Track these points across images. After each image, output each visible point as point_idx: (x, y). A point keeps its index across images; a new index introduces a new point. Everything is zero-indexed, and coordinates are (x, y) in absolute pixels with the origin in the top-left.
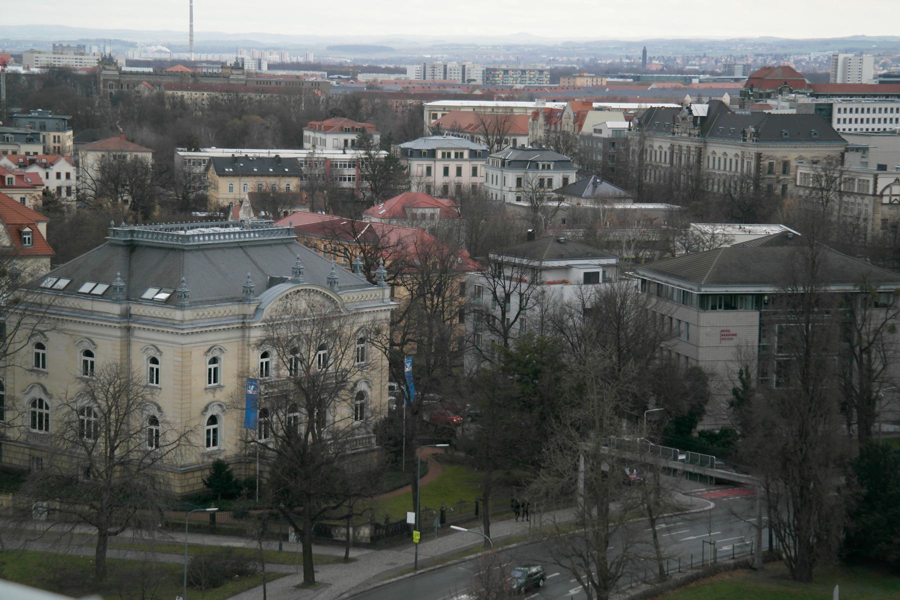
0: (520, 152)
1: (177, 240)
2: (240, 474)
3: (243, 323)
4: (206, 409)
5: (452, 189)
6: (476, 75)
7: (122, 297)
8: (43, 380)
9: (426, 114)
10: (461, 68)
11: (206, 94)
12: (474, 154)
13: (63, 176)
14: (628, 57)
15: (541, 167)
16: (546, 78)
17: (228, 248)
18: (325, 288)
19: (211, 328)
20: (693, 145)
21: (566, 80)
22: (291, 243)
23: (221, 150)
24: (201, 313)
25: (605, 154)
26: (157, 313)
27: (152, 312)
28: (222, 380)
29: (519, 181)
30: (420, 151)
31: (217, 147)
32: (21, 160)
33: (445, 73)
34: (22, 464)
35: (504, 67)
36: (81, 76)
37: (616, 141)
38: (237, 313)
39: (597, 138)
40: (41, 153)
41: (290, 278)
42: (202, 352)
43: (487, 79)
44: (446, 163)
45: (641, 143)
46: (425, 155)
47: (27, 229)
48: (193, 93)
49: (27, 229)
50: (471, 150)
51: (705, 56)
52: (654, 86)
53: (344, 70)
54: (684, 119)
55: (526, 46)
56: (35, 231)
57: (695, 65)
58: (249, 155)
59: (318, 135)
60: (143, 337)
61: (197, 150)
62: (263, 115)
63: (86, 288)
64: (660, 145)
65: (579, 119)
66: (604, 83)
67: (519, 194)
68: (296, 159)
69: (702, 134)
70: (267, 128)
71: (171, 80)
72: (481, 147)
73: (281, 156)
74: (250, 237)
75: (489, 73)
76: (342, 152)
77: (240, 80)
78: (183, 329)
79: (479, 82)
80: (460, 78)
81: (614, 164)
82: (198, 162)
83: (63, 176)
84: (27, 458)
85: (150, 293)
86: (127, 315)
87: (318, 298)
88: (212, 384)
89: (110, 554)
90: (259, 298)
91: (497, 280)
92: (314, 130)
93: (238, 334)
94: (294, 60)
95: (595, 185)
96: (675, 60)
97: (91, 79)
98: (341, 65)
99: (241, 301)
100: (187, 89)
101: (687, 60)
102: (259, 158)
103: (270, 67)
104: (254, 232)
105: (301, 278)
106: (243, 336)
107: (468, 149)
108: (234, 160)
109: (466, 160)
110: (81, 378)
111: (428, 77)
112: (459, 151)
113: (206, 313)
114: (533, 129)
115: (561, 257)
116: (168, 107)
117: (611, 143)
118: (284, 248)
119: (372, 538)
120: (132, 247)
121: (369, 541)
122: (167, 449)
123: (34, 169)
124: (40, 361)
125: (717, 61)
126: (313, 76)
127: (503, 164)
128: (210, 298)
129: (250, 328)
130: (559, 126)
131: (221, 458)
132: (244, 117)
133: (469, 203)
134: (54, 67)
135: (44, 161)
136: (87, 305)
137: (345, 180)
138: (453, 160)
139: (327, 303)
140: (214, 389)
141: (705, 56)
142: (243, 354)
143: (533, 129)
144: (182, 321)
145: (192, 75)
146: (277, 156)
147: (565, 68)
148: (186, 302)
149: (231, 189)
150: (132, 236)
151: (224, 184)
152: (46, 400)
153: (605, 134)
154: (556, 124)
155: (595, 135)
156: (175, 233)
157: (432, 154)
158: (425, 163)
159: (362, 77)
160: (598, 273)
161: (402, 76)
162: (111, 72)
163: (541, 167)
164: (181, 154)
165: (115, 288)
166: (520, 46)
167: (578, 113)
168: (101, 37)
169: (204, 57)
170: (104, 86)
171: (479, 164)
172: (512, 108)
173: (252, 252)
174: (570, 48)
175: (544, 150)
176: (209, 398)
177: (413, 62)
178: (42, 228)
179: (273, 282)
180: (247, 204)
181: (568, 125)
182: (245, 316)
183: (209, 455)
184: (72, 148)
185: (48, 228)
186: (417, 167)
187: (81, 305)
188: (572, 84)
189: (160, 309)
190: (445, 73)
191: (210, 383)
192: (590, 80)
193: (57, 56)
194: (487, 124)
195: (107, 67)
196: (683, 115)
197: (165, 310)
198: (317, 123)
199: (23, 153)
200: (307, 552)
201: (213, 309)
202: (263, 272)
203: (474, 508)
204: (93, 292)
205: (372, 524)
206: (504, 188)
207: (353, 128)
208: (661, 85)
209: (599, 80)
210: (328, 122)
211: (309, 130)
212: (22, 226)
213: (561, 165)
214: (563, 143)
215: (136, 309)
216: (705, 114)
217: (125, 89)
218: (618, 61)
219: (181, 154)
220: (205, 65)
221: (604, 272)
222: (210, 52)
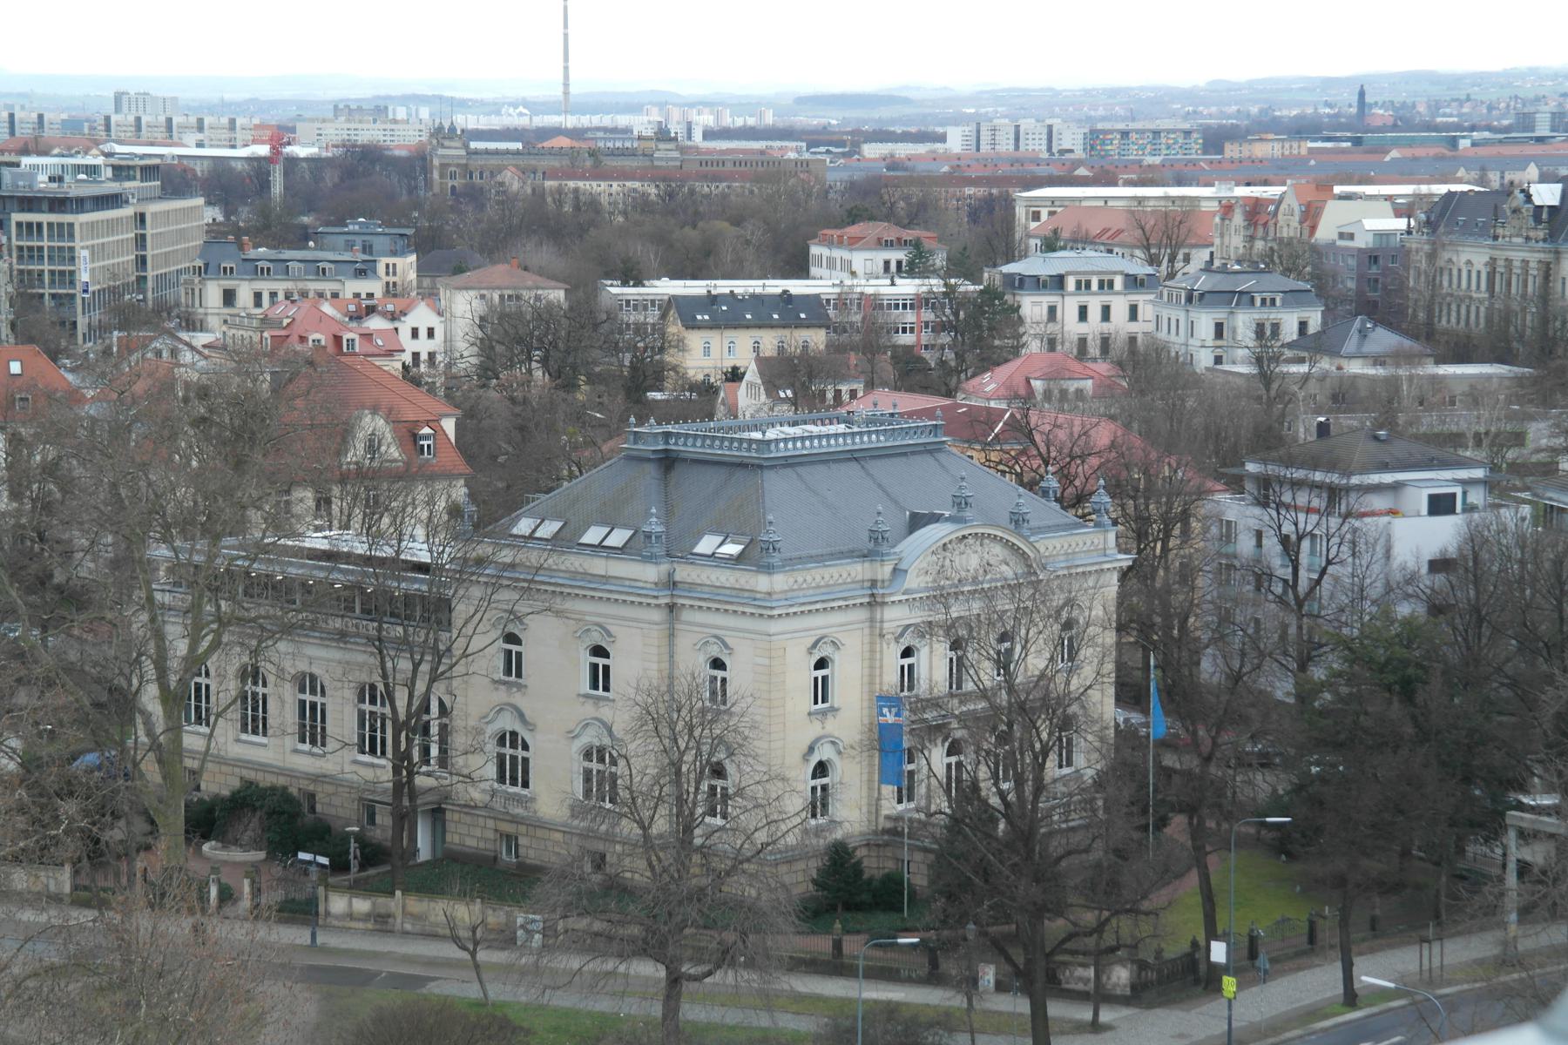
0: (1219, 277)
1: (749, 450)
2: (874, 866)
3: (873, 595)
4: (811, 749)
5: (1118, 346)
6: (1072, 139)
7: (659, 550)
8: (518, 699)
9: (1020, 212)
10: (1045, 131)
11: (615, 184)
12: (1134, 283)
13: (423, 333)
14: (1327, 104)
15: (1258, 302)
16: (1196, 142)
17: (834, 461)
18: (1005, 529)
19: (818, 606)
20: (1534, 258)
21: (1236, 147)
22: (939, 450)
23: (681, 283)
24: (800, 579)
25: (1361, 277)
26: (723, 579)
27: (713, 577)
28: (836, 697)
29: (1219, 330)
30: (1037, 278)
31: (671, 278)
32: (352, 308)
33: (1017, 139)
34: (482, 845)
35: (1121, 126)
36: (395, 161)
37: (1380, 258)
38: (859, 577)
39: (1347, 249)
40: (378, 294)
41: (947, 514)
42: (804, 649)
43: (1092, 148)
44: (1083, 299)
45: (1432, 256)
46: (1045, 286)
47: (426, 430)
48: (594, 184)
49: (426, 430)
50: (1127, 275)
51: (1468, 99)
52: (1394, 154)
53: (836, 137)
54: (1516, 211)
55: (1142, 89)
56: (439, 432)
57: (1451, 115)
58: (737, 291)
59: (837, 253)
60: (698, 623)
61: (639, 283)
62: (737, 221)
63: (593, 536)
64: (1470, 259)
65: (1311, 215)
66: (1304, 152)
67: (1219, 352)
68: (817, 296)
69: (1552, 236)
70: (748, 242)
71: (555, 163)
72: (1141, 269)
73: (793, 291)
74: (862, 442)
75: (1095, 138)
76: (888, 282)
77: (672, 159)
78: (772, 608)
79: (1079, 153)
80: (1044, 147)
81: (1376, 291)
82: (642, 305)
83: (423, 333)
84: (490, 835)
85: (706, 545)
86: (671, 584)
87: (997, 549)
88: (820, 705)
89: (692, 1012)
90: (896, 550)
91: (1283, 512)
92: (830, 243)
93: (862, 614)
94: (739, 122)
95: (1363, 334)
96: (1414, 106)
97: (417, 163)
98: (825, 129)
99: (866, 556)
100: (583, 178)
101: (1435, 106)
102: (754, 296)
103: (708, 134)
104: (869, 433)
105: (968, 514)
106: (872, 620)
107: (1121, 273)
108: (712, 300)
109: (1118, 293)
110: (587, 696)
111: (985, 148)
112: (1106, 278)
113: (809, 579)
114: (1222, 235)
115: (1385, 467)
116: (567, 208)
117: (1372, 257)
118: (928, 459)
119: (1133, 987)
120: (668, 462)
121: (1128, 992)
122: (784, 827)
123: (375, 323)
124: (513, 665)
125: (1490, 108)
126: (792, 151)
127: (1189, 299)
128: (813, 552)
129: (884, 604)
130: (1272, 230)
131: (838, 835)
132: (701, 224)
133: (1144, 368)
134: (354, 146)
135: (390, 307)
136: (598, 566)
137: (904, 330)
138: (1095, 294)
139: (1012, 560)
140: (824, 713)
141: (1468, 99)
142: (872, 651)
143: (1222, 235)
144: (769, 594)
145: (594, 154)
146: (785, 292)
147: (1221, 126)
148: (776, 559)
149: (707, 351)
150: (667, 443)
151: (695, 340)
152: (523, 733)
153: (1362, 242)
154: (1265, 225)
155: (1340, 243)
156: (746, 435)
157: (1058, 282)
158: (1046, 300)
159: (872, 151)
160: (1454, 495)
161: (939, 146)
162: (454, 151)
163: (1258, 302)
164: (614, 290)
165: (648, 536)
166: (1132, 89)
167: (1309, 205)
168: (409, 91)
169: (595, 120)
170: (442, 176)
171: (1141, 299)
172: (1197, 199)
173: (877, 467)
174: (1220, 92)
175: (1262, 271)
176: (815, 729)
177: (957, 120)
178: (449, 426)
179: (917, 522)
180: (752, 375)
181: (1288, 226)
182: (874, 583)
183: (818, 831)
184: (415, 283)
185: (459, 427)
186: (1032, 307)
187: (586, 565)
188: (1246, 154)
189: (728, 572)
190: (1017, 139)
191: (816, 702)
192: (1277, 146)
193: (352, 126)
194: (1147, 228)
195: (447, 143)
196: (1514, 204)
197: (738, 574)
198: (836, 233)
199: (349, 295)
200: (1039, 1014)
201: (821, 571)
202: (896, 502)
203: (1306, 930)
204: (606, 543)
205: (1133, 962)
206: (1191, 341)
207: (899, 239)
208: (1408, 152)
209: (1295, 145)
210: (853, 230)
211: (821, 243)
212: (417, 424)
213: (1294, 298)
214: (1301, 264)
215: (684, 573)
216: (1555, 201)
217: (477, 180)
218: (1310, 111)
219: (614, 290)
220: (600, 134)
221: (1465, 493)
222: (594, 112)
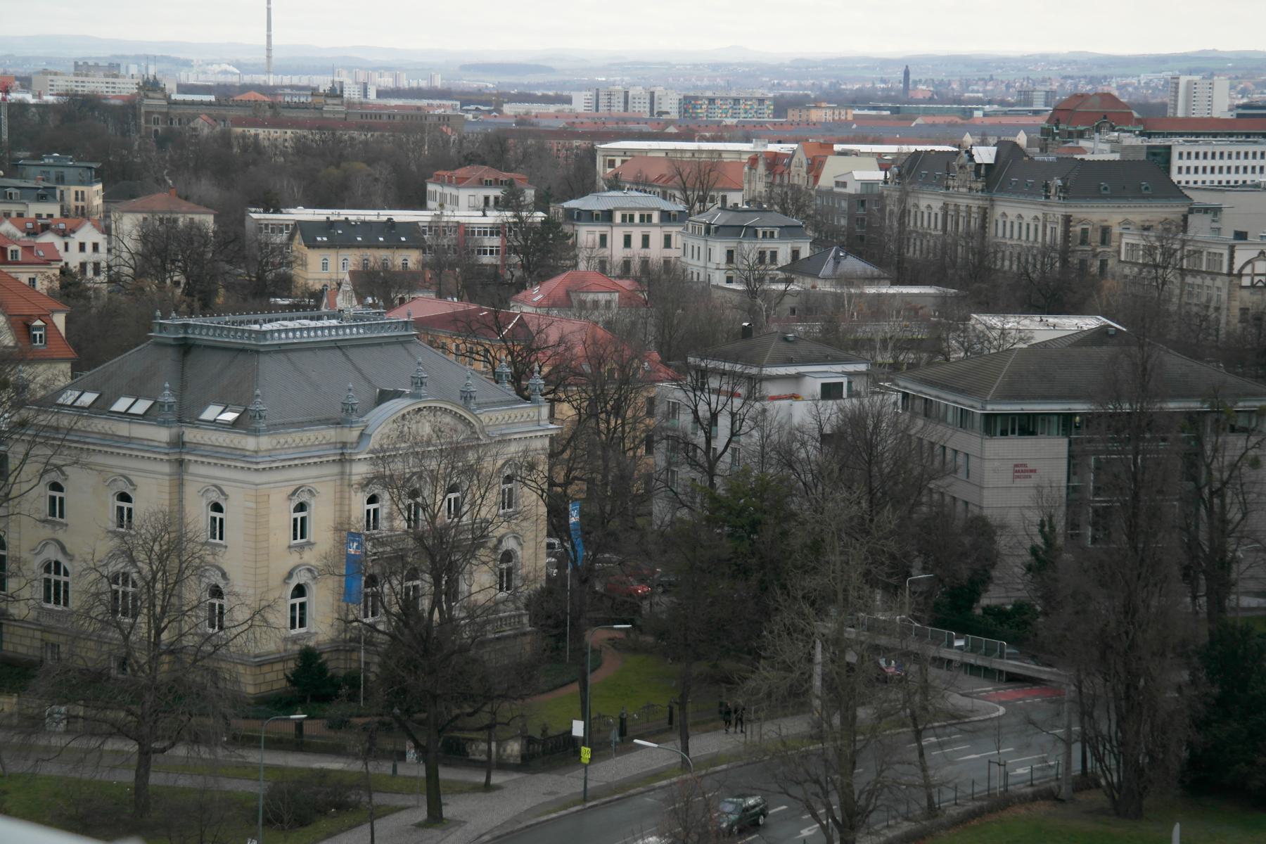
0: (731, 214)
1: (249, 338)
2: (337, 666)
3: (342, 454)
4: (290, 575)
5: (636, 266)
6: (670, 105)
7: (171, 417)
8: (61, 535)
9: (600, 161)
10: (648, 96)
11: (289, 132)
12: (667, 217)
13: (89, 248)
14: (883, 81)
15: (760, 235)
16: (768, 109)
17: (320, 349)
18: (458, 405)
19: (296, 462)
20: (975, 204)
21: (797, 112)
22: (410, 342)
23: (311, 211)
24: (282, 441)
25: (851, 217)
26: (221, 440)
27: (213, 438)
28: (312, 534)
29: (730, 254)
30: (590, 212)
31: (306, 207)
32: (30, 225)
33: (626, 102)
34: (31, 652)
35: (709, 94)
36: (113, 107)
37: (867, 199)
38: (333, 440)
39: (840, 194)
40: (57, 215)
41: (408, 391)
42: (285, 495)
43: (686, 111)
44: (628, 229)
45: (902, 201)
46: (597, 219)
47: (38, 323)
48: (272, 131)
49: (38, 323)
50: (662, 211)
51: (991, 78)
52: (919, 121)
53: (484, 98)
54: (962, 167)
55: (739, 64)
56: (50, 326)
57: (978, 92)
58: (350, 218)
59: (448, 190)
60: (201, 473)
61: (277, 211)
62: (370, 162)
63: (121, 405)
64: (929, 204)
65: (815, 167)
66: (850, 117)
67: (730, 273)
68: (416, 223)
69: (988, 188)
70: (376, 180)
71: (240, 113)
72: (677, 206)
73: (396, 219)
74: (351, 333)
75: (688, 103)
76: (481, 213)
77: (338, 112)
78: (257, 463)
79: (674, 115)
80: (647, 109)
81: (864, 230)
82: (278, 228)
83: (89, 248)
84: (38, 644)
85: (211, 413)
86: (178, 443)
87: (448, 419)
88: (299, 541)
89: (155, 779)
90: (364, 419)
91: (698, 393)
92: (442, 183)
93: (335, 469)
94: (414, 84)
95: (837, 260)
96: (949, 84)
97: (128, 111)
98: (480, 92)
99: (338, 423)
100: (262, 126)
101: (966, 84)
102: (364, 223)
103: (380, 94)
104: (357, 326)
105: (423, 391)
106: (342, 473)
107: (658, 209)
108: (329, 225)
109: (655, 225)
110: (114, 532)
111: (602, 109)
112: (646, 213)
113: (290, 440)
114: (749, 182)
115: (789, 362)
116: (236, 150)
117: (860, 201)
118: (399, 348)
119: (523, 757)
120: (185, 347)
121: (519, 761)
122: (235, 631)
123: (48, 238)
124: (56, 508)
125: (1008, 86)
126: (440, 107)
127: (708, 231)
128: (295, 419)
129: (352, 461)
130: (786, 178)
131: (311, 644)
132: (344, 165)
133: (660, 285)
134: (76, 95)
135: (62, 226)
136: (123, 429)
137: (485, 253)
138: (637, 225)
139: (460, 427)
140: (302, 547)
141: (991, 78)
142: (342, 498)
143: (749, 182)
144: (256, 452)
145: (270, 106)
146: (389, 220)
147: (795, 95)
148: (262, 425)
149: (325, 266)
150: (186, 332)
151: (314, 258)
152: (65, 563)
153: (852, 189)
154: (781, 174)
155: (837, 190)
156: (246, 327)
157: (607, 216)
158: (598, 230)
159: (509, 109)
160: (841, 384)
161: (566, 107)
162: (156, 102)
163: (760, 235)
164: (255, 216)
165: (162, 405)
166: (731, 64)
167: (813, 159)
168: (141, 53)
169: (286, 80)
170: (147, 122)
171: (674, 230)
172: (720, 152)
173: (354, 354)
174: (801, 67)
175: (765, 210)
176: (294, 559)
177: (580, 87)
178: (59, 320)
179: (384, 396)
180: (347, 287)
181: (798, 176)
182: (344, 445)
183: (295, 640)
184: (101, 208)
185: (68, 321)
186: (587, 234)
187: (114, 428)
188: (804, 118)
189: (225, 435)
190: (626, 102)
191: (295, 538)
192: (829, 112)
193: (80, 79)
194: (685, 174)
195: (151, 94)
196: (961, 162)
197: (232, 436)
198: (446, 174)
199: (32, 215)
200: (432, 777)
201: (300, 434)
202: (369, 382)
203: (667, 715)
204: (131, 411)
205: (523, 737)
206: (709, 265)
207: (496, 180)
208: (930, 120)
209: (843, 112)
210: (461, 172)
211: (435, 182)
212: (31, 317)
213: (789, 232)
214: (791, 202)
215: (191, 435)
216: (991, 160)
217: (176, 125)
218: (869, 85)
219: (255, 216)
220: (288, 91)
221: (850, 383)
222: (295, 73)
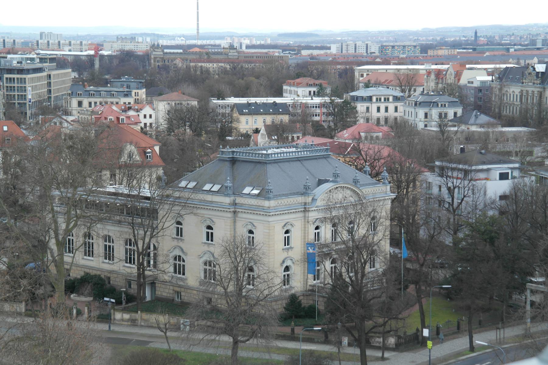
0: (426, 97)
1: (262, 157)
2: (305, 302)
3: (305, 208)
4: (283, 262)
5: (391, 121)
6: (374, 49)
7: (230, 192)
8: (181, 244)
9: (357, 74)
10: (365, 46)
11: (215, 64)
12: (396, 99)
13: (148, 116)
14: (464, 36)
15: (440, 105)
16: (418, 50)
17: (292, 161)
18: (351, 185)
19: (286, 212)
20: (536, 90)
21: (432, 51)
22: (328, 157)
23: (238, 99)
24: (280, 202)
25: (475, 97)
26: (253, 202)
27: (249, 202)
28: (292, 244)
29: (426, 115)
30: (362, 97)
31: (235, 97)
32: (123, 107)
33: (355, 49)
34: (168, 295)
35: (392, 44)
36: (138, 56)
37: (482, 90)
38: (300, 202)
39: (471, 87)
40: (132, 103)
41: (331, 179)
42: (281, 227)
43: (382, 52)
44: (379, 104)
45: (500, 89)
46: (365, 100)
47: (149, 150)
48: (208, 64)
49: (149, 150)
50: (394, 96)
51: (513, 35)
52: (487, 54)
53: (292, 48)
54: (530, 74)
55: (399, 31)
56: (153, 151)
57: (507, 40)
58: (257, 102)
59: (293, 89)
60: (244, 218)
61: (223, 99)
62: (258, 77)
63: (207, 187)
64: (514, 90)
65: (458, 75)
66: (456, 53)
67: (426, 123)
68: (286, 103)
69: (542, 83)
70: (261, 85)
71: (194, 57)
72: (399, 94)
73: (277, 102)
74: (301, 154)
75: (383, 48)
76: (310, 98)
77: (235, 56)
78: (270, 212)
79: (377, 54)
80: (365, 52)
81: (481, 102)
82: (224, 107)
83: (148, 116)
84: (171, 292)
85: (247, 190)
86: (235, 204)
87: (349, 192)
88: (287, 246)
89: (242, 354)
90: (313, 192)
91: (448, 179)
92: (290, 85)
93: (301, 215)
94: (258, 43)
95: (476, 117)
96: (494, 37)
97: (146, 57)
98: (288, 45)
99: (303, 194)
100: (204, 62)
101: (502, 37)
102: (263, 103)
103: (248, 47)
104: (304, 151)
105: (338, 179)
106: (305, 217)
107: (392, 95)
108: (249, 105)
109: (391, 102)
110: (205, 243)
111: (344, 52)
112: (387, 97)
113: (283, 202)
114: (427, 82)
115: (484, 163)
116: (198, 73)
117: (479, 90)
118: (324, 160)
119: (396, 345)
120: (233, 161)
121: (394, 346)
122: (274, 289)
123: (131, 113)
124: (179, 232)
125: (521, 38)
126: (277, 53)
127: (416, 104)
128: (284, 193)
129: (309, 211)
130: (444, 80)
131: (293, 291)
132: (245, 78)
133: (400, 129)
134: (124, 51)
135: (136, 107)
136: (209, 198)
137: (316, 115)
138: (383, 103)
139: (354, 195)
140: (288, 249)
141: (513, 35)
142: (305, 227)
143: (427, 82)
144: (269, 207)
145: (208, 54)
146: (274, 102)
147: (427, 44)
148: (271, 195)
149: (247, 123)
150: (233, 155)
151: (243, 119)
152: (183, 256)
153: (476, 84)
154: (442, 78)
155: (468, 85)
156: (261, 152)
157: (370, 99)
158: (366, 105)
159: (305, 53)
160: (508, 173)
161: (328, 51)
162: (159, 53)
163: (440, 105)
164: (215, 101)
165: (227, 187)
166: (396, 31)
167: (457, 72)
168: (143, 32)
169: (208, 42)
170: (154, 61)
171: (399, 104)
172: (418, 69)
173: (306, 163)
174: (426, 32)
175: (441, 95)
176: (285, 255)
177: (334, 42)
178: (157, 149)
179: (320, 182)
180: (263, 131)
181: (450, 79)
182: (305, 204)
183: (286, 290)
184: (145, 99)
185: (160, 149)
186: (361, 107)
187: (205, 198)
188: (435, 54)
189: (254, 200)
190: (355, 49)
191: (285, 245)
192: (446, 51)
193: (123, 44)
194: (401, 79)
195: (156, 50)
196: (529, 71)
197: (258, 200)
198: (292, 81)
199: (122, 103)
200: (363, 354)
201: (287, 199)
202: (313, 175)
203: (456, 325)
204: (212, 190)
205: (396, 336)
206: (416, 119)
207: (314, 84)
208: (492, 53)
209: (453, 51)
210: (298, 80)
211: (287, 85)
212: (146, 148)
213: (452, 104)
214: (455, 92)
215: (239, 200)
216: (544, 70)
217: (167, 63)
218: (458, 39)
219: (215, 101)
220: (210, 47)
221: (512, 172)
222: (208, 39)
